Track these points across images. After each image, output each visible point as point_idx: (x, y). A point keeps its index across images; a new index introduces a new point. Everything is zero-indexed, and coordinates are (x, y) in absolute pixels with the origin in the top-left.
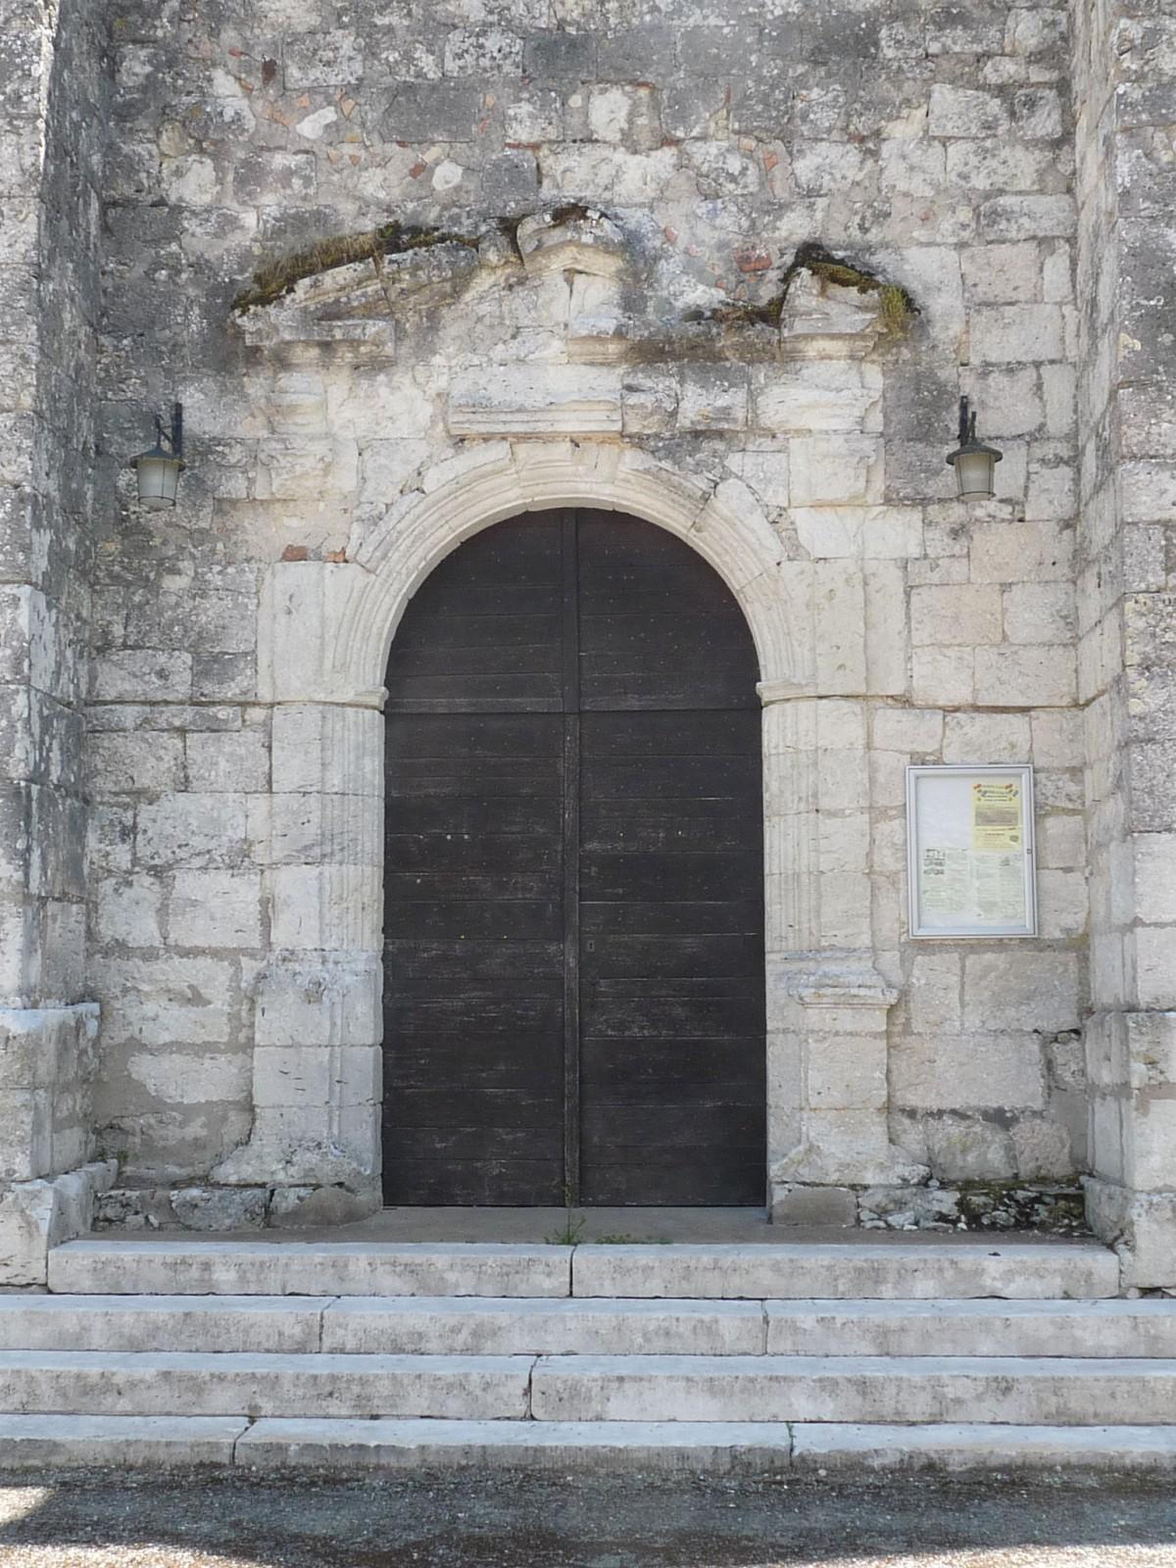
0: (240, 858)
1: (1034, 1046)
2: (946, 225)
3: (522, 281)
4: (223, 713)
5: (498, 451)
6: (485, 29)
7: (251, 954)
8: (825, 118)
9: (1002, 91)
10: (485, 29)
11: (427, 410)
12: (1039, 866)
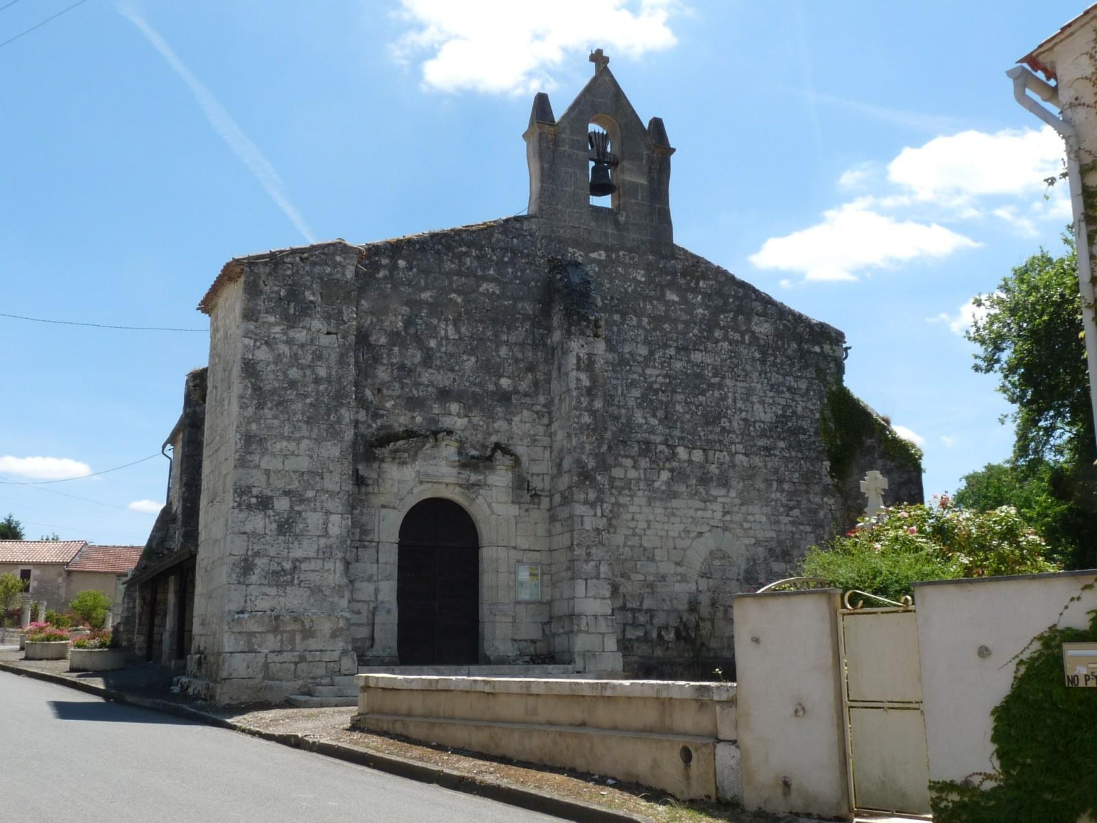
0: (370, 579)
1: (540, 626)
2: (525, 441)
3: (436, 446)
4: (367, 544)
5: (429, 485)
6: (428, 386)
7: (372, 602)
8: (501, 415)
9: (537, 413)
10: (428, 386)
11: (414, 474)
12: (542, 586)
